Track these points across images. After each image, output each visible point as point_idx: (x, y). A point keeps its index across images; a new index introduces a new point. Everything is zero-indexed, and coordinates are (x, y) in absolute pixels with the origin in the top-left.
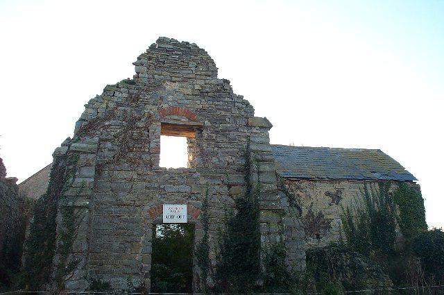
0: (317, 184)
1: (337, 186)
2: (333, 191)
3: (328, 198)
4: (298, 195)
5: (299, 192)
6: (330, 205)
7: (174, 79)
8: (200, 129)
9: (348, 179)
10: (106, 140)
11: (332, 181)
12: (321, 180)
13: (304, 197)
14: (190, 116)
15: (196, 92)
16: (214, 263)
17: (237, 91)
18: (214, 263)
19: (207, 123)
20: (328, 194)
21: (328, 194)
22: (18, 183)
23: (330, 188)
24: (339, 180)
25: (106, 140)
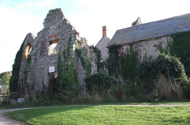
0: (150, 42)
1: (160, 40)
2: (158, 44)
3: (155, 48)
4: (140, 49)
5: (140, 48)
6: (156, 51)
7: (52, 24)
8: (58, 40)
9: (165, 36)
10: (38, 50)
11: (156, 38)
12: (150, 39)
13: (143, 49)
14: (55, 36)
15: (58, 27)
16: (92, 74)
17: (19, 50)
18: (92, 74)
19: (60, 37)
20: (155, 46)
21: (155, 46)
22: (95, 46)
23: (156, 42)
24: (160, 37)
25: (38, 50)
